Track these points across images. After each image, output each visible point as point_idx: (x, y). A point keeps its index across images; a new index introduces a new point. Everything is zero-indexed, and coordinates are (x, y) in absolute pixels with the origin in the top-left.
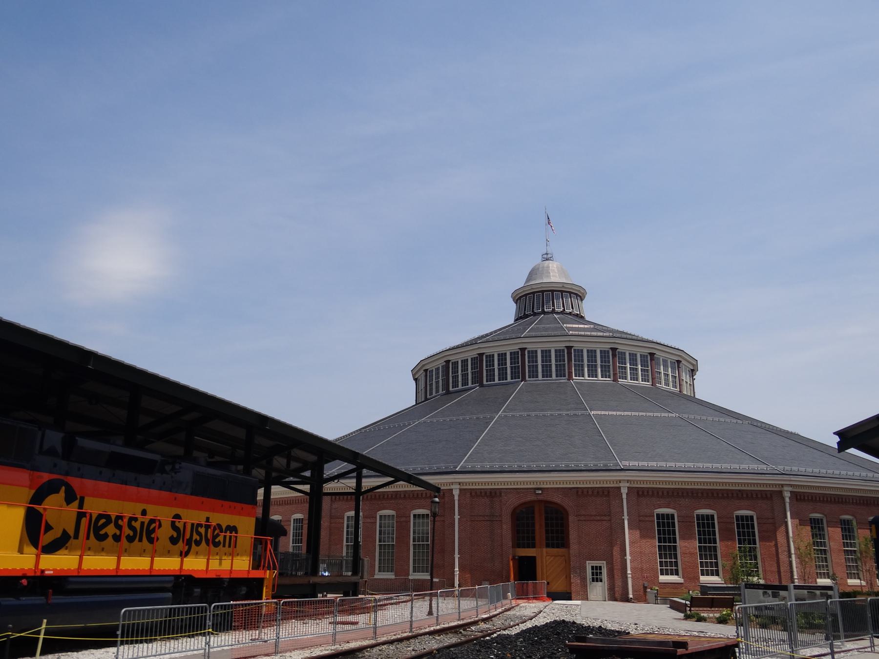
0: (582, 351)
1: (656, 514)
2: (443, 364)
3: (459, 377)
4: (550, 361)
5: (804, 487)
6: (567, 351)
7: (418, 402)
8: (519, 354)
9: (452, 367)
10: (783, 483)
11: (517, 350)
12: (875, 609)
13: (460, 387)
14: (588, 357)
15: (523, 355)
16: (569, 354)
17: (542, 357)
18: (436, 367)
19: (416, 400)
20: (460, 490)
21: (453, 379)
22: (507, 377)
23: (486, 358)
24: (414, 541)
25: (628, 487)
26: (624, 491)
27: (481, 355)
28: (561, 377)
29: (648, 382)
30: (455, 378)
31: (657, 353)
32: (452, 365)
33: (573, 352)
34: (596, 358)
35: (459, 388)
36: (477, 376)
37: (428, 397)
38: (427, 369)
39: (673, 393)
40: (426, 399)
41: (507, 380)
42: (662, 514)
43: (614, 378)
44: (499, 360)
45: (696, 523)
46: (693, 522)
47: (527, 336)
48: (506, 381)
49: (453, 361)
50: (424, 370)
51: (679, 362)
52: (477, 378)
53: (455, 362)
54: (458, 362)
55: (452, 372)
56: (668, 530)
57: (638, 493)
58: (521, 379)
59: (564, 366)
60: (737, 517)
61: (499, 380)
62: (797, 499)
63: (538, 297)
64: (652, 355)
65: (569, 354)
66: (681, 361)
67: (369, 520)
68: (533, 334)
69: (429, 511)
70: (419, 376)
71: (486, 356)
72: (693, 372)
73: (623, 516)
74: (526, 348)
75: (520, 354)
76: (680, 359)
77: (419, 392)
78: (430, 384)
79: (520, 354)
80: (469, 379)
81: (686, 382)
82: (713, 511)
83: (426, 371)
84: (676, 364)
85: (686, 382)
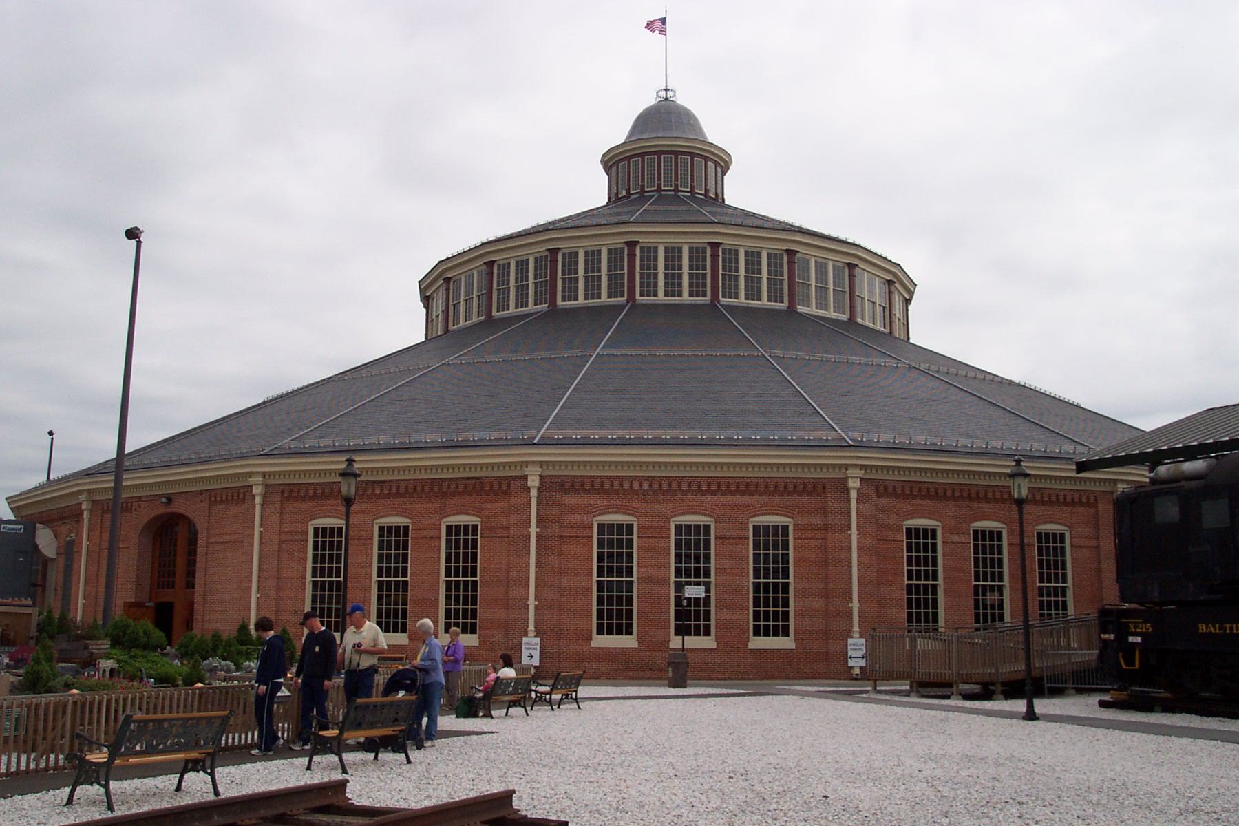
0: (736, 252)
1: (907, 529)
2: (480, 269)
3: (511, 292)
4: (737, 270)
5: (1055, 480)
6: (788, 258)
7: (429, 337)
8: (723, 258)
9: (498, 274)
10: (1115, 477)
11: (622, 246)
12: (96, 710)
13: (512, 310)
14: (768, 266)
15: (632, 256)
16: (715, 256)
17: (666, 259)
18: (468, 274)
19: (427, 335)
20: (267, 486)
21: (498, 295)
22: (600, 293)
23: (564, 258)
24: (380, 575)
25: (541, 476)
26: (534, 482)
27: (554, 252)
28: (650, 296)
29: (782, 302)
30: (504, 293)
31: (802, 249)
32: (499, 270)
33: (720, 254)
34: (760, 266)
35: (510, 311)
36: (546, 290)
37: (451, 327)
38: (450, 278)
39: (836, 322)
40: (446, 331)
41: (600, 298)
42: (990, 531)
43: (712, 296)
44: (586, 262)
45: (972, 544)
46: (416, 538)
47: (640, 220)
48: (599, 301)
49: (501, 262)
50: (444, 279)
51: (890, 283)
52: (546, 294)
53: (504, 264)
54: (509, 264)
55: (498, 282)
56: (983, 558)
57: (877, 488)
58: (625, 298)
59: (782, 284)
60: (909, 530)
61: (586, 298)
62: (879, 496)
63: (636, 164)
64: (791, 253)
65: (715, 256)
66: (1077, 473)
67: (955, 538)
68: (648, 218)
69: (344, 522)
70: (434, 291)
71: (564, 254)
72: (908, 302)
73: (537, 533)
74: (638, 242)
75: (626, 253)
76: (854, 261)
77: (432, 321)
78: (454, 305)
79: (626, 253)
80: (530, 294)
81: (899, 320)
82: (1000, 525)
83: (447, 280)
84: (847, 271)
85: (899, 320)
